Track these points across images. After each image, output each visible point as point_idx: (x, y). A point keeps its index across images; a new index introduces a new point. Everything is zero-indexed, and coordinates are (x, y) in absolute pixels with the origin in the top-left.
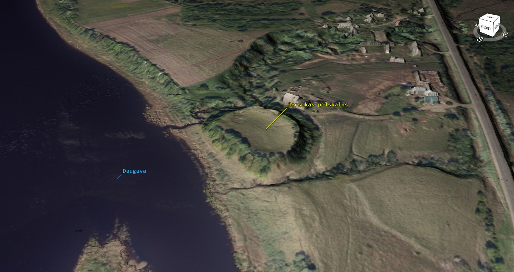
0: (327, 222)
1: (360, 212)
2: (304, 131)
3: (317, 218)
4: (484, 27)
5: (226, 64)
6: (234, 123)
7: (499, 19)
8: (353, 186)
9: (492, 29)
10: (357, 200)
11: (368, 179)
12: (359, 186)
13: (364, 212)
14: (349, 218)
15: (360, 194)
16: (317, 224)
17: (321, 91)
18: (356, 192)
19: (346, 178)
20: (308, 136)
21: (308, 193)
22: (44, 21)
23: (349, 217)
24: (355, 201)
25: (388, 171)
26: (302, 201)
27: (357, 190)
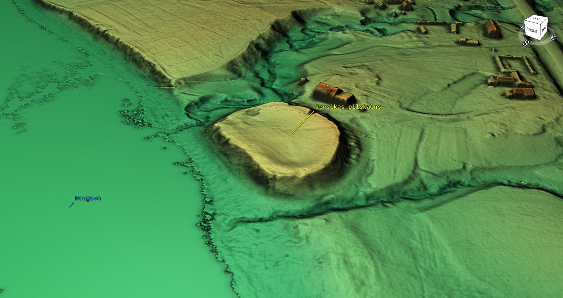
0: (388, 276)
1: (437, 260)
2: (347, 136)
3: (372, 270)
4: (531, 30)
5: (237, 49)
6: (246, 125)
7: (547, 21)
8: (423, 217)
9: (539, 32)
10: (431, 240)
11: (445, 207)
12: (432, 217)
13: (443, 260)
14: (421, 270)
15: (435, 231)
16: (372, 279)
17: (368, 81)
18: (428, 227)
19: (413, 204)
20: (352, 144)
21: (355, 229)
22: (322, 101)
23: (421, 267)
24: (428, 242)
25: (474, 195)
26: (347, 242)
27: (431, 225)
